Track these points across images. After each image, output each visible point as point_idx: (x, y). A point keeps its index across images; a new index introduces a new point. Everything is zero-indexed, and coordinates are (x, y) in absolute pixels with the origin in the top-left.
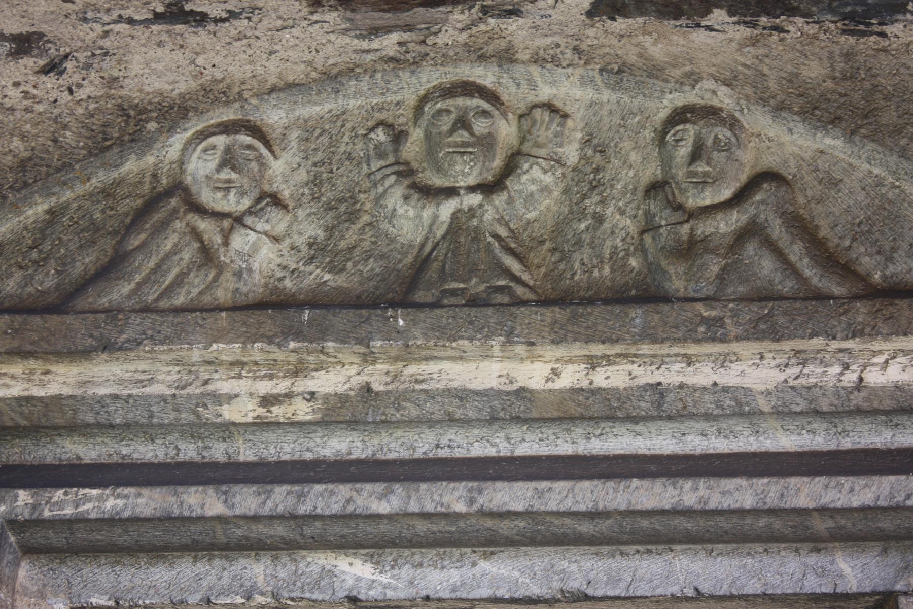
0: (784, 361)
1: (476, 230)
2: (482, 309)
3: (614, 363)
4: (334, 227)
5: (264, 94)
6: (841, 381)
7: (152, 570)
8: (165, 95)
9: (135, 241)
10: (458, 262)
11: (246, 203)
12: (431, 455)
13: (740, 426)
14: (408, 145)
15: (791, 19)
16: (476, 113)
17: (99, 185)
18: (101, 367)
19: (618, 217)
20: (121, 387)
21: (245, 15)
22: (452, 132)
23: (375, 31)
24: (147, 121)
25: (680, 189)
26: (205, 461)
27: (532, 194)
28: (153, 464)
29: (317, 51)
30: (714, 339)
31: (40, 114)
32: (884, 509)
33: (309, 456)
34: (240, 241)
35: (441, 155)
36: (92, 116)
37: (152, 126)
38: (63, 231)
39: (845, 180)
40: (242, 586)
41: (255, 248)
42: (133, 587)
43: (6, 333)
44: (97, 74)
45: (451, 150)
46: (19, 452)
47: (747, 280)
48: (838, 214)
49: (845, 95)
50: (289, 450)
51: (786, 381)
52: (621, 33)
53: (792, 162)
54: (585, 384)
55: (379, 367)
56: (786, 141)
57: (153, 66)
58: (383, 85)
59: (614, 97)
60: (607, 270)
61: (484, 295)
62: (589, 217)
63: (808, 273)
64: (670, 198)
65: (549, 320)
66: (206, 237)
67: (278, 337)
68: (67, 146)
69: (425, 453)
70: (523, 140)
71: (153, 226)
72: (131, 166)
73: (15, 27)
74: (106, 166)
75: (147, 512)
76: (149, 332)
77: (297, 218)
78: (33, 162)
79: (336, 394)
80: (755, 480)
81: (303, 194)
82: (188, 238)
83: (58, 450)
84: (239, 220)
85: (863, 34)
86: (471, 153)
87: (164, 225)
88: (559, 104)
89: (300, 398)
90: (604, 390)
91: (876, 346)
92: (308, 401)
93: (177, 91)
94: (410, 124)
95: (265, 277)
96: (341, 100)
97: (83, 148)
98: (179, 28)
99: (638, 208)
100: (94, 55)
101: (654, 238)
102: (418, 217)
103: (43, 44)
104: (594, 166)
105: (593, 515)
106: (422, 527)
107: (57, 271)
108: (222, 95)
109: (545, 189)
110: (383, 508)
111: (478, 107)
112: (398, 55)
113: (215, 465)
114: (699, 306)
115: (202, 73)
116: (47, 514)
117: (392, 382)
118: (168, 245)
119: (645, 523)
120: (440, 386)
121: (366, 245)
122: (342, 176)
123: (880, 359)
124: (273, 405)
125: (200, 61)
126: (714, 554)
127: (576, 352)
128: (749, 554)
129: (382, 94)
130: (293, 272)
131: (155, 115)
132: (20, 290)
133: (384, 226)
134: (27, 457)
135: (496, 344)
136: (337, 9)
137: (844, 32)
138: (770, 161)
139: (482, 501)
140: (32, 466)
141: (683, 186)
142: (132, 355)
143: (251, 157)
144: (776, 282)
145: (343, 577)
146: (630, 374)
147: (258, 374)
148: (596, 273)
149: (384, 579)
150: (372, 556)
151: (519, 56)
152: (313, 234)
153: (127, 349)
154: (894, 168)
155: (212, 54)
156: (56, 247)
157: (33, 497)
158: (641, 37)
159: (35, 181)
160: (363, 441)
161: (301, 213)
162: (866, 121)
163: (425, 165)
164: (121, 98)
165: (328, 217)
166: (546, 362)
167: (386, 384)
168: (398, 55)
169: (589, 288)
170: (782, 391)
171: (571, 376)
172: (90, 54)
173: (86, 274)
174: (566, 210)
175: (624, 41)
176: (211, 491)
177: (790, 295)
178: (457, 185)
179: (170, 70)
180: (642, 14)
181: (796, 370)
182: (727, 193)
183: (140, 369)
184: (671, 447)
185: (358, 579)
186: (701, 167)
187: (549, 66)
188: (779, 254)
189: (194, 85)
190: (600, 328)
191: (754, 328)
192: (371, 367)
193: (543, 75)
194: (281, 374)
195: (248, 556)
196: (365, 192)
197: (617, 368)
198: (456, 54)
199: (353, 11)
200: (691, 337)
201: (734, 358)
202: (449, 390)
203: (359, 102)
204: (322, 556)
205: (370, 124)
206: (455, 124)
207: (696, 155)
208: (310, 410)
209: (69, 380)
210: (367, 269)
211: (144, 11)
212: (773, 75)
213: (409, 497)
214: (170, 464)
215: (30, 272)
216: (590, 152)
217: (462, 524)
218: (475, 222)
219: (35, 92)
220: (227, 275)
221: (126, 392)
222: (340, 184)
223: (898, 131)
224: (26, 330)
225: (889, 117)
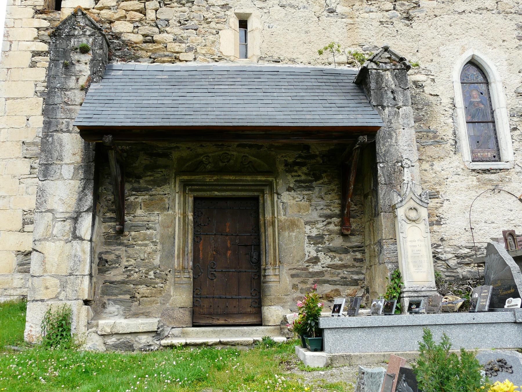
72: (198, 159)
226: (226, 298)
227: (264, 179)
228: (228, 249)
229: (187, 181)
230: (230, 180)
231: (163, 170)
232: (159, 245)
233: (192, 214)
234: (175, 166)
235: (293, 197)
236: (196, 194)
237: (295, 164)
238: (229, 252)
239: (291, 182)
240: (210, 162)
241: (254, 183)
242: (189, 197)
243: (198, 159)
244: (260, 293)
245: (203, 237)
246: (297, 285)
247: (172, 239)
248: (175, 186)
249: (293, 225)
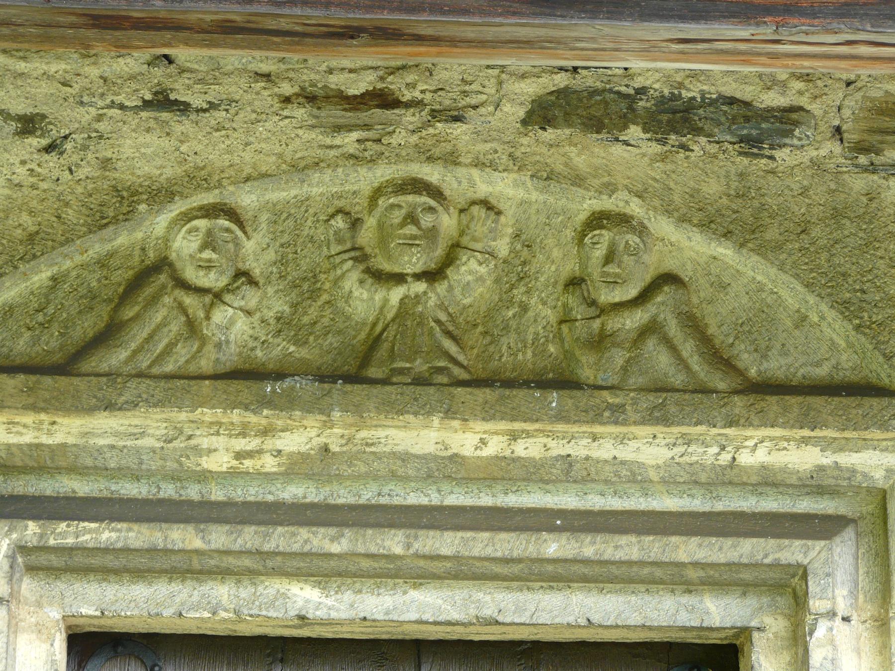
0: (672, 441)
1: (421, 315)
2: (426, 388)
3: (532, 436)
4: (297, 304)
5: (240, 182)
6: (717, 460)
7: (133, 587)
8: (154, 179)
9: (129, 313)
10: (405, 344)
11: (223, 282)
12: (373, 502)
13: (632, 489)
14: (363, 231)
15: (696, 139)
16: (424, 209)
17: (95, 256)
18: (101, 421)
19: (540, 307)
20: (117, 439)
21: (223, 107)
22: (402, 225)
23: (338, 129)
24: (139, 202)
25: (594, 287)
26: (182, 498)
27: (468, 283)
28: (137, 500)
29: (287, 145)
30: (616, 423)
31: (45, 191)
32: (746, 565)
33: (270, 498)
34: (220, 315)
35: (392, 246)
36: (91, 195)
37: (142, 207)
38: (64, 298)
39: (733, 284)
40: (209, 603)
41: (232, 322)
42: (117, 601)
43: (23, 391)
44: (94, 155)
45: (401, 242)
46: (21, 486)
47: (647, 372)
48: (724, 315)
49: (738, 212)
50: (253, 493)
51: (673, 458)
52: (551, 142)
53: (689, 266)
54: (507, 453)
55: (335, 430)
56: (687, 247)
57: (143, 150)
58: (343, 177)
59: (542, 197)
60: (529, 354)
61: (427, 375)
62: (516, 305)
63: (696, 368)
64: (586, 294)
65: (481, 400)
66: (190, 311)
67: (253, 404)
68: (69, 223)
69: (368, 500)
70: (462, 233)
71: (144, 299)
72: (123, 239)
73: (20, 107)
74: (102, 240)
76: (145, 396)
77: (267, 293)
78: (40, 236)
79: (299, 453)
80: (643, 538)
81: (272, 273)
82: (175, 312)
83: (57, 485)
84: (218, 296)
85: (756, 156)
86: (418, 245)
87: (154, 300)
89: (269, 454)
90: (523, 458)
91: (749, 432)
92: (275, 456)
93: (164, 176)
94: (365, 212)
95: (239, 347)
96: (305, 188)
97: (83, 225)
98: (165, 115)
99: (558, 300)
100: (90, 137)
101: (570, 329)
103: (46, 125)
104: (522, 259)
106: (365, 564)
107: (61, 334)
108: (204, 182)
109: (480, 279)
110: (335, 548)
111: (425, 203)
112: (357, 152)
113: (190, 503)
114: (605, 393)
115: (186, 160)
116: (52, 542)
117: (347, 444)
118: (158, 317)
119: (550, 568)
120: (387, 449)
121: (326, 321)
122: (305, 257)
124: (245, 458)
125: (184, 148)
126: (604, 591)
127: (502, 427)
128: (633, 592)
129: (342, 184)
130: (263, 343)
131: (145, 197)
132: (29, 349)
133: (341, 304)
134: (30, 489)
135: (436, 421)
136: (305, 107)
137: (740, 154)
138: (671, 265)
139: (417, 546)
140: (34, 497)
141: (596, 285)
142: (129, 414)
143: (228, 239)
144: (670, 375)
145: (295, 599)
146: (545, 446)
147: (233, 432)
148: (520, 356)
150: (320, 583)
151: (461, 159)
152: (280, 309)
153: (126, 409)
154: (774, 278)
155: (195, 142)
156: (59, 312)
157: (40, 528)
158: (567, 148)
159: (42, 255)
160: (317, 488)
161: (270, 290)
162: (753, 237)
163: (377, 251)
164: (114, 179)
165: (293, 295)
166: (475, 433)
167: (341, 446)
168: (357, 152)
169: (514, 370)
170: (669, 466)
171: (495, 446)
172: (86, 136)
173: (85, 337)
174: (497, 298)
175: (552, 150)
176: (190, 528)
177: (681, 387)
178: (405, 271)
179: (157, 155)
180: (570, 126)
181: (682, 449)
182: (632, 292)
183: (132, 423)
184: (575, 504)
185: (307, 601)
186: (612, 269)
187: (488, 170)
188: (673, 349)
189: (179, 171)
190: (523, 409)
191: (650, 415)
192: (329, 431)
193: (481, 176)
194: (253, 433)
195: (216, 579)
196: (325, 273)
197: (535, 440)
198: (408, 155)
199: (319, 108)
200: (597, 419)
201: (631, 436)
202: (394, 453)
203: (321, 190)
204: (278, 581)
205: (331, 210)
206: (405, 219)
207: (609, 258)
208: (276, 463)
209: (74, 431)
210: (327, 343)
211: (134, 98)
212: (678, 189)
213: (357, 540)
214: (152, 500)
215: (37, 333)
216: (519, 247)
217: (399, 563)
218: (420, 308)
219: (39, 170)
220: (209, 348)
221: (121, 443)
223: (778, 247)
224: (39, 389)
225: (772, 234)
230: (449, 468)
240: (243, 276)
241: (697, 503)
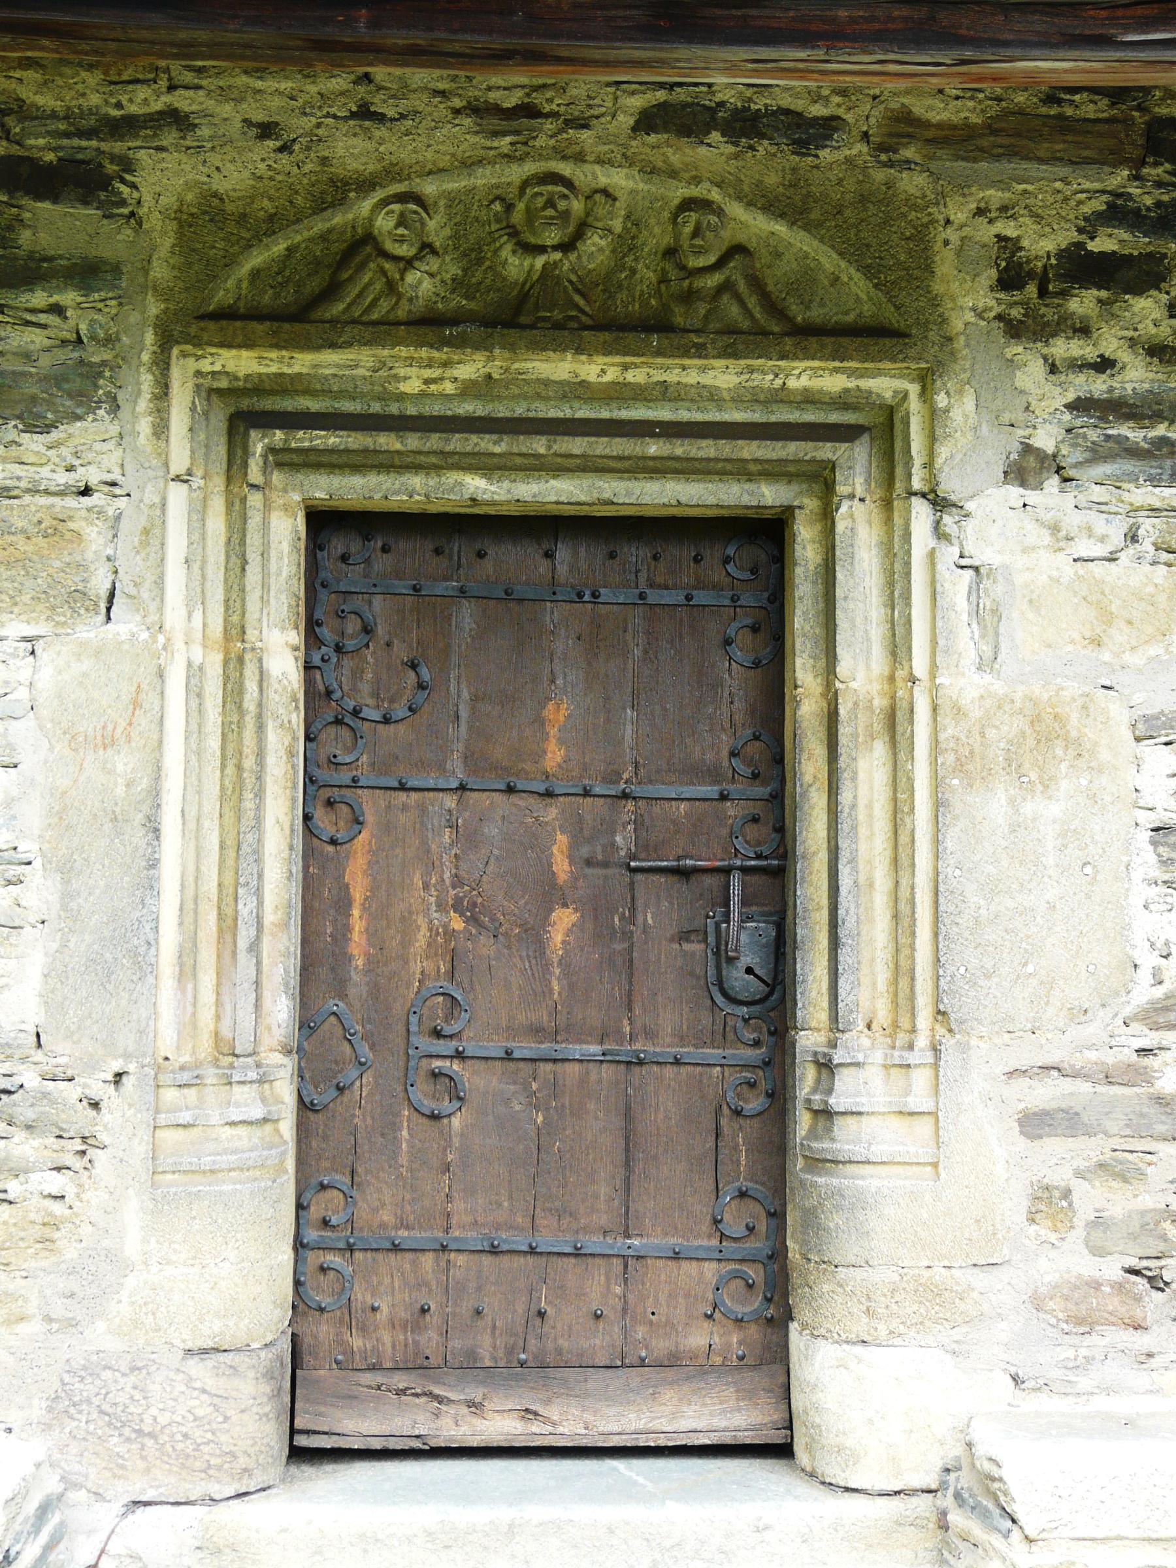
11: (413, 251)
13: (711, 406)
22: (544, 208)
23: (496, 134)
24: (350, 191)
30: (700, 357)
33: (449, 413)
34: (412, 277)
37: (352, 195)
41: (420, 282)
54: (621, 380)
56: (753, 224)
60: (637, 306)
63: (758, 316)
70: (588, 214)
72: (338, 219)
75: (355, 447)
85: (804, 155)
87: (362, 266)
88: (611, 190)
91: (796, 364)
96: (472, 180)
102: (522, 265)
105: (620, 458)
109: (601, 250)
110: (497, 450)
113: (392, 416)
114: (692, 336)
116: (293, 445)
118: (366, 279)
119: (651, 463)
123: (796, 372)
125: (382, 149)
133: (499, 269)
135: (569, 356)
137: (793, 153)
138: (741, 238)
149: (493, 488)
161: (448, 259)
171: (612, 375)
176: (393, 435)
180: (667, 132)
181: (747, 376)
182: (712, 259)
186: (698, 242)
189: (379, 167)
200: (686, 354)
207: (696, 233)
212: (747, 181)
220: (404, 302)
222: (472, 239)
223: (819, 225)
225: (815, 215)
226: (532, 1251)
227: (833, 382)
228: (550, 894)
229: (258, 387)
230: (579, 390)
231: (68, 297)
232: (35, 875)
233: (295, 637)
234: (160, 271)
235: (1055, 529)
236: (326, 488)
237: (1082, 268)
238: (564, 919)
239: (1041, 409)
240: (427, 248)
242: (267, 507)
243: (338, 219)
244: (778, 1216)
245: (371, 805)
246: (1067, 1194)
247: (139, 837)
248: (161, 430)
249: (1047, 736)
